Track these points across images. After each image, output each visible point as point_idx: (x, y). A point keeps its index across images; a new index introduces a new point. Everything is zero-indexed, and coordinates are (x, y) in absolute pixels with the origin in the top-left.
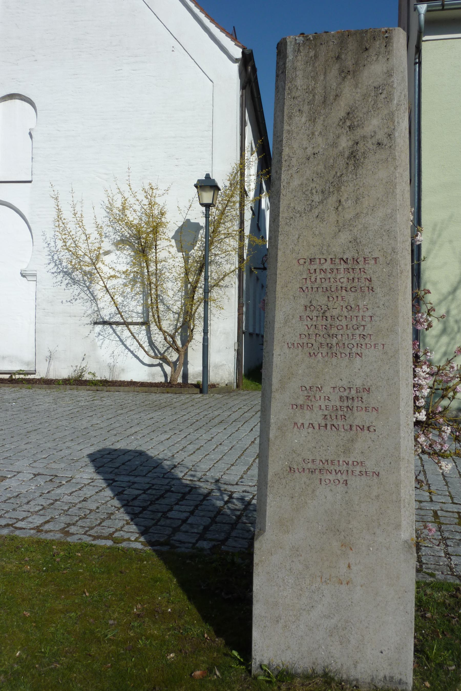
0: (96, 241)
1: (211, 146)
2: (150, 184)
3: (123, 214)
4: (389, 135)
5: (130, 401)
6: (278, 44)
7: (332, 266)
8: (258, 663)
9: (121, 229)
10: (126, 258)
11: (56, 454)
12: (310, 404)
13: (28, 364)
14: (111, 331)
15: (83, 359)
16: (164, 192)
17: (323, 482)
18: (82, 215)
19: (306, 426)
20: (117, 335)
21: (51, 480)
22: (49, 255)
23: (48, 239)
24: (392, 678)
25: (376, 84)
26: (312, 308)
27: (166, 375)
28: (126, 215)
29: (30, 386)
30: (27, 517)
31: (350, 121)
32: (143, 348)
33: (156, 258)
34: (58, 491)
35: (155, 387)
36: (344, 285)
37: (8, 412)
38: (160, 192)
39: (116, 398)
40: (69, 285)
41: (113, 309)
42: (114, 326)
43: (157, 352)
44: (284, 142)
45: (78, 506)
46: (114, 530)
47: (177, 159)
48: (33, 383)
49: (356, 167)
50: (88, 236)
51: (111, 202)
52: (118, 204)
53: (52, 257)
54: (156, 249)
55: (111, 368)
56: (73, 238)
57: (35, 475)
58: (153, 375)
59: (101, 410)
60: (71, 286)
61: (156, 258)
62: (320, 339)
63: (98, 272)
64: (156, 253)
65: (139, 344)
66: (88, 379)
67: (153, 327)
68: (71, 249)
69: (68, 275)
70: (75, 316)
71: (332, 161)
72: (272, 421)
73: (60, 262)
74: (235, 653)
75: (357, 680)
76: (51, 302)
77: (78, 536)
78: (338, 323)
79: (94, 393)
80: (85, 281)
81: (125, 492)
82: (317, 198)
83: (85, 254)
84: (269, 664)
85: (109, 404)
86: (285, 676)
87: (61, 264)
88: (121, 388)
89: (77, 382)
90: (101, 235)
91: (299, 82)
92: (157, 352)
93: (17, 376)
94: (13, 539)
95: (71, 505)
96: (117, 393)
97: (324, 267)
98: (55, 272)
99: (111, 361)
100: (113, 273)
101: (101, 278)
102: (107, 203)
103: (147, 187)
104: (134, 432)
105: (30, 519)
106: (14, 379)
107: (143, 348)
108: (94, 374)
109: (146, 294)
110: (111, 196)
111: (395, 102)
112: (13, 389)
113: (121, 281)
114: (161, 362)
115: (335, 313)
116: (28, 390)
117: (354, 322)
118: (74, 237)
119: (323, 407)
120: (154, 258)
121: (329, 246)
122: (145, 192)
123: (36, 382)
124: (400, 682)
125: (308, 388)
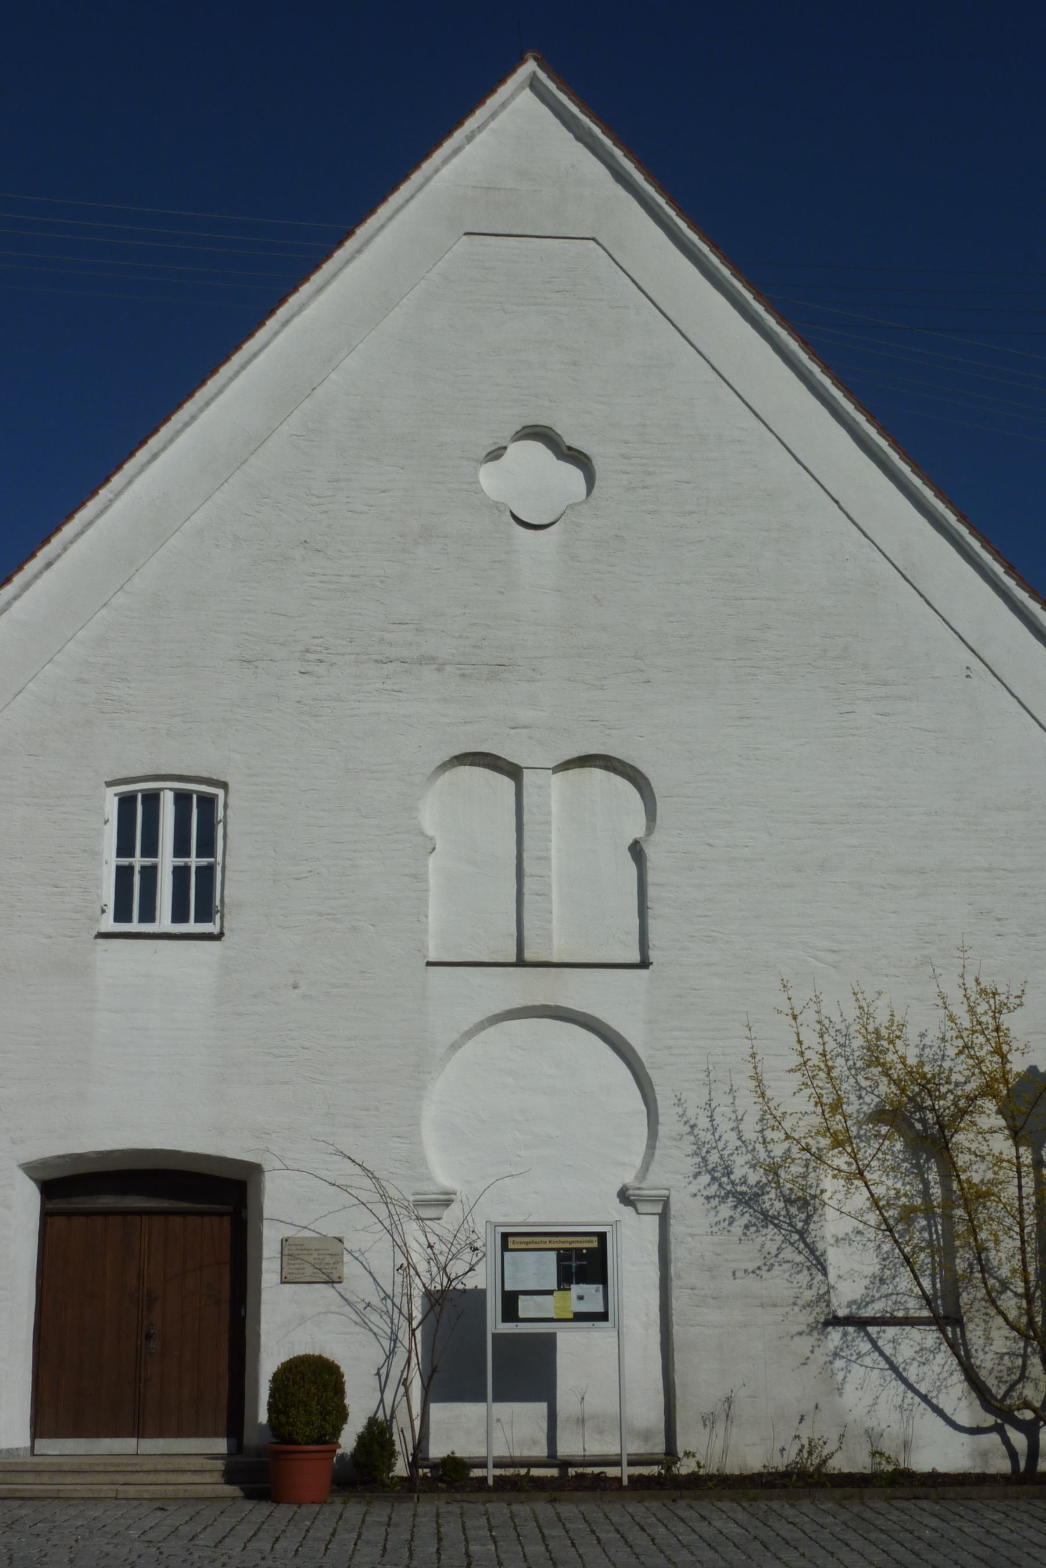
14: (865, 1346)
20: (882, 1354)
22: (696, 1154)
23: (691, 1113)
27: (1013, 1454)
40: (753, 1229)
47: (999, 920)
53: (703, 1158)
58: (984, 1455)
60: (757, 1231)
69: (747, 1203)
70: (775, 1305)
87: (729, 1174)
89: (801, 1482)
98: (714, 1197)
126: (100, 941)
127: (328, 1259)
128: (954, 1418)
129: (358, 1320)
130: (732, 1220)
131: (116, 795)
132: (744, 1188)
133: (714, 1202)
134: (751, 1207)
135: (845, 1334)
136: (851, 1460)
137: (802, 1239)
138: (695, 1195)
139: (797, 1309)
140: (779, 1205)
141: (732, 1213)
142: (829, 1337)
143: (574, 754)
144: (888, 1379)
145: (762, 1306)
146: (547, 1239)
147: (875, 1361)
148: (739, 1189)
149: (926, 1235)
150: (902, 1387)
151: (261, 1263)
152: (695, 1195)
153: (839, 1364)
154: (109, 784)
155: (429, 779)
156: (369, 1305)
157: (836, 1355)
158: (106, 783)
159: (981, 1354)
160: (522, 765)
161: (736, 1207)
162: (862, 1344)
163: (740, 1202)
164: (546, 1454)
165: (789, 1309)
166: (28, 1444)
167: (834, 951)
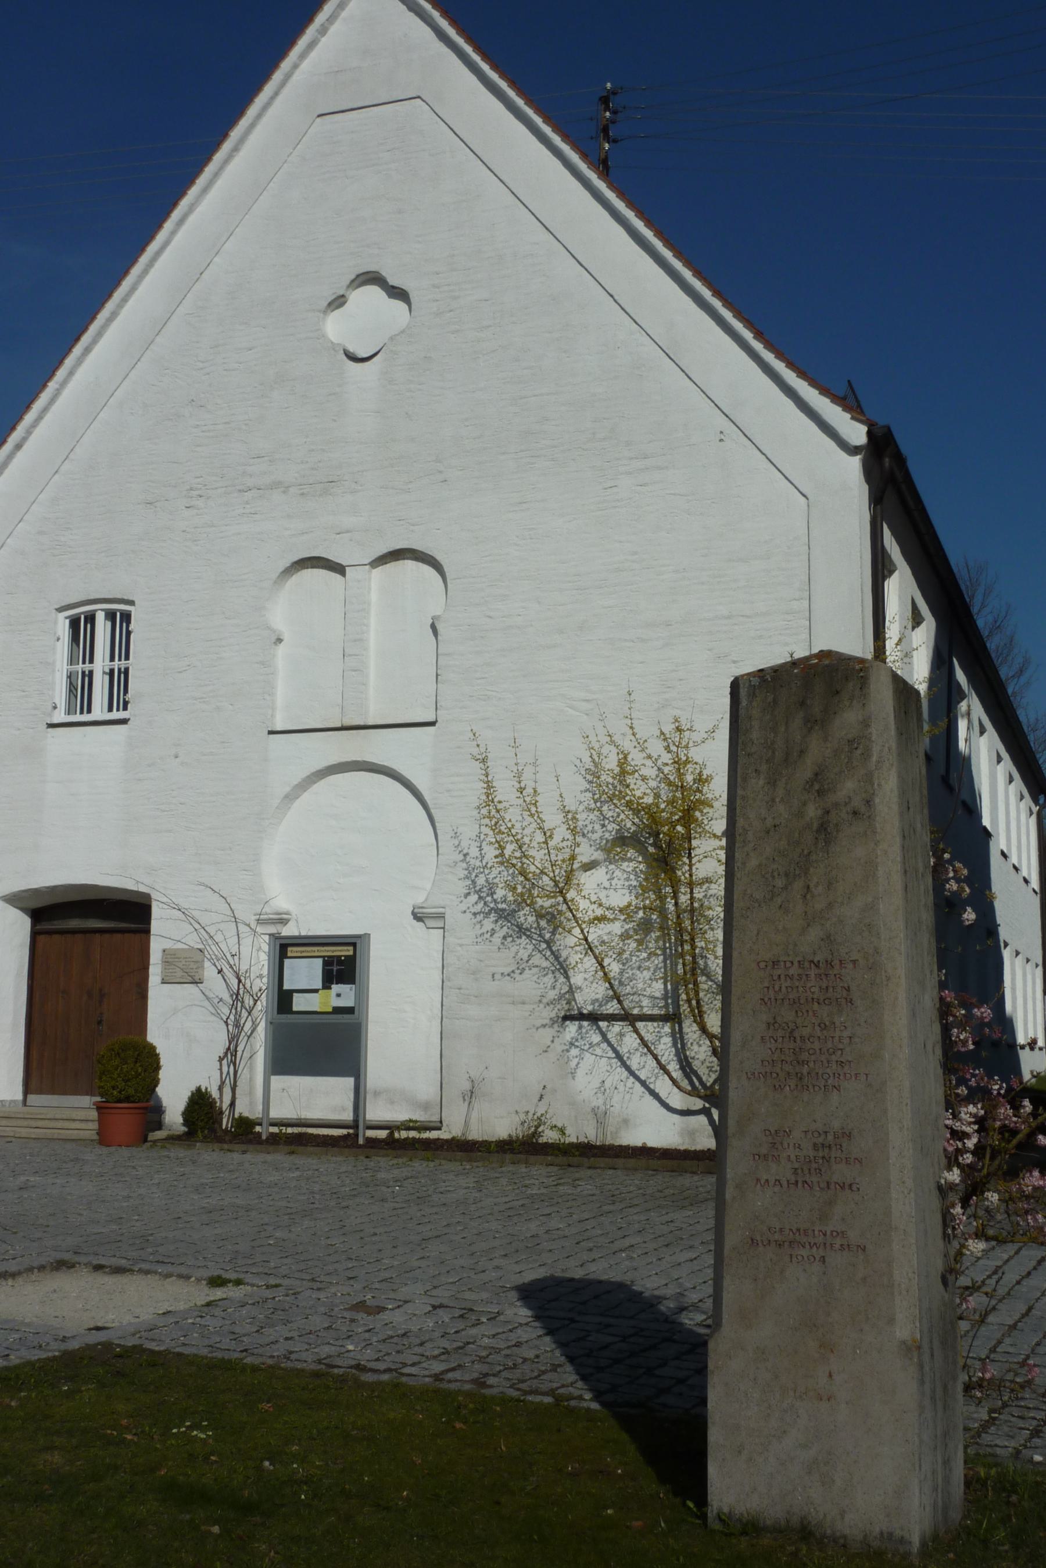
0: (565, 843)
1: (807, 631)
2: (676, 721)
3: (620, 782)
4: (868, 802)
5: (632, 1188)
6: (732, 683)
7: (800, 971)
8: (715, 1512)
9: (618, 816)
10: (628, 879)
11: (475, 1277)
12: (776, 1154)
13: (426, 1106)
14: (596, 1038)
15: (541, 1097)
16: (706, 736)
17: (794, 1259)
18: (535, 791)
19: (771, 1183)
21: (462, 1316)
22: (467, 877)
23: (464, 844)
24: (890, 1534)
25: (850, 737)
26: (776, 1025)
28: (628, 786)
29: (429, 1154)
30: (420, 1363)
31: (819, 784)
32: (667, 1073)
33: (691, 875)
34: (473, 1331)
35: (692, 1159)
36: (815, 996)
37: (386, 1205)
38: (696, 737)
39: (606, 1181)
40: (509, 939)
41: (600, 990)
42: (603, 1024)
43: (697, 1084)
44: (738, 811)
45: (503, 1352)
46: (559, 1385)
47: (734, 662)
48: (437, 1149)
49: (828, 842)
50: (548, 834)
51: (597, 759)
52: (611, 762)
53: (473, 881)
54: (690, 857)
55: (600, 1117)
56: (517, 841)
57: (434, 1307)
58: (691, 1134)
59: (569, 1204)
60: (513, 941)
61: (691, 875)
62: (788, 1068)
63: (569, 908)
64: (691, 866)
65: (659, 1062)
66: (550, 1141)
67: (691, 1029)
68: (514, 861)
69: (505, 918)
70: (524, 1003)
71: (797, 835)
72: (728, 1176)
73: (490, 889)
74: (691, 1504)
75: (845, 1537)
76: (474, 973)
77: (498, 1385)
78: (809, 1045)
79: (561, 1172)
80: (541, 929)
81: (590, 1338)
82: (779, 883)
83: (542, 872)
84: (730, 1513)
85: (590, 1192)
86: (751, 1527)
88: (620, 1162)
89: (526, 1148)
90: (573, 831)
91: (755, 735)
92: (697, 1084)
93: (404, 1134)
94: (397, 1385)
95: (493, 1351)
96: (611, 1172)
97: (791, 972)
98: (479, 913)
99: (598, 1102)
100: (599, 912)
101: (577, 922)
102: (587, 760)
103: (668, 728)
104: (628, 1244)
105: (424, 1365)
106: (398, 1140)
107: (667, 1073)
108: (562, 1131)
109: (671, 957)
110: (596, 746)
111: (874, 759)
112: (395, 1161)
113: (617, 928)
114: (707, 1105)
115: (805, 1032)
116: (425, 1164)
117: (830, 1045)
118: (519, 837)
119: (793, 1157)
120: (687, 875)
121: (796, 945)
122: (665, 740)
123: (442, 1146)
124: (902, 1540)
125: (773, 1132)
126: (50, 730)
127: (192, 965)
128: (667, 1101)
129: (213, 1011)
130: (493, 932)
131: (66, 618)
132: (504, 906)
133: (480, 917)
134: (509, 922)
135: (580, 1027)
136: (581, 1130)
137: (549, 947)
138: (465, 912)
139: (542, 1006)
140: (531, 919)
141: (493, 926)
142: (567, 1029)
143: (384, 550)
144: (614, 1066)
145: (513, 1003)
146: (315, 949)
147: (604, 1050)
148: (500, 906)
149: (661, 943)
150: (626, 1073)
151: (148, 968)
152: (465, 912)
153: (574, 1052)
154: (60, 610)
155: (275, 582)
156: (221, 1000)
157: (572, 1044)
158: (57, 610)
159: (695, 1047)
160: (344, 564)
161: (496, 921)
162: (594, 1036)
163: (500, 917)
164: (351, 1118)
165: (535, 1006)
166: (20, 1097)
167: (587, 701)
